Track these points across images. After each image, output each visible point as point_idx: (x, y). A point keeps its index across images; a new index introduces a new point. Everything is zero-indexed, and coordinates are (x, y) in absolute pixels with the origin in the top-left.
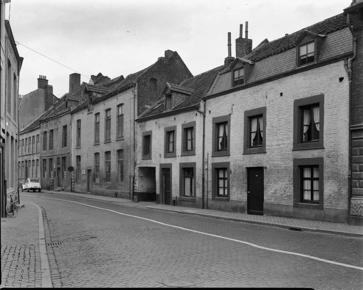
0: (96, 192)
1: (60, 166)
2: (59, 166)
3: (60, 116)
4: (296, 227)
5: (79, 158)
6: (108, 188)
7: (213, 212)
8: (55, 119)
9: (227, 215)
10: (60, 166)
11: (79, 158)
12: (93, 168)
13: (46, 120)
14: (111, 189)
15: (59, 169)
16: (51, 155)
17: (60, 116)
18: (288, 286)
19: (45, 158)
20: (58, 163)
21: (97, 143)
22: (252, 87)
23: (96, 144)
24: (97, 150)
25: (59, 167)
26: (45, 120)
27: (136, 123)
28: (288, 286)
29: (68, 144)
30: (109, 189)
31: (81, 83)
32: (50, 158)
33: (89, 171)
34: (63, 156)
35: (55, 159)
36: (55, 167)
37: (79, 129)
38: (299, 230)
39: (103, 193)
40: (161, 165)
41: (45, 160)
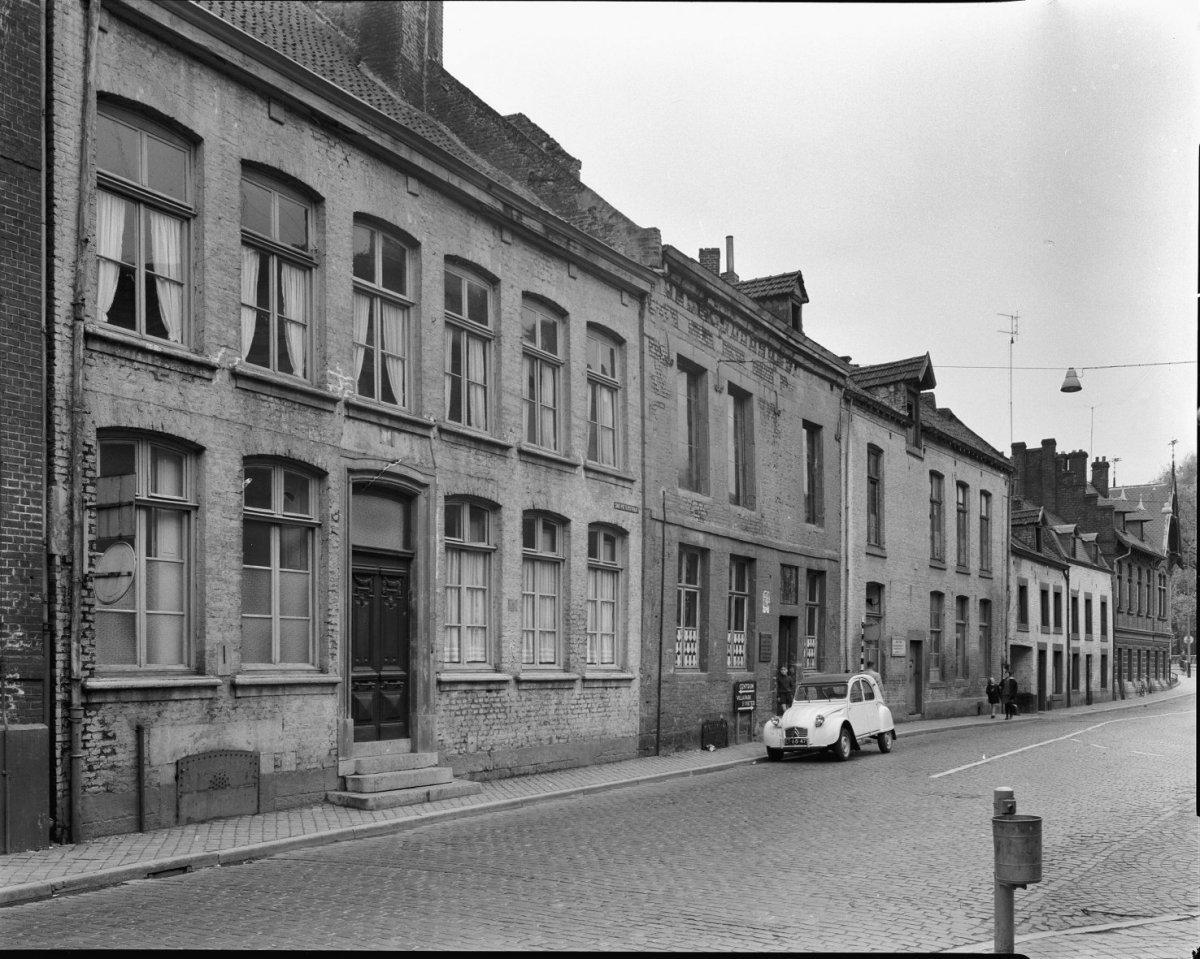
0: (936, 709)
1: (800, 611)
2: (789, 610)
3: (799, 359)
4: (176, 862)
5: (875, 590)
6: (964, 695)
7: (243, 829)
8: (763, 343)
9: (153, 849)
10: (800, 611)
11: (875, 590)
12: (927, 639)
13: (716, 298)
14: (969, 696)
15: (787, 623)
16: (747, 536)
17: (799, 359)
18: (709, 947)
19: (700, 539)
20: (788, 592)
21: (937, 563)
22: (216, 40)
23: (936, 564)
24: (937, 582)
25: (789, 614)
26: (709, 294)
27: (1012, 559)
28: (709, 947)
29: (829, 512)
30: (966, 696)
31: (1008, 454)
32: (741, 551)
33: (916, 645)
34: (814, 565)
35: (769, 566)
36: (766, 610)
37: (875, 481)
38: (183, 868)
39: (954, 709)
40: (1039, 643)
41: (694, 556)
